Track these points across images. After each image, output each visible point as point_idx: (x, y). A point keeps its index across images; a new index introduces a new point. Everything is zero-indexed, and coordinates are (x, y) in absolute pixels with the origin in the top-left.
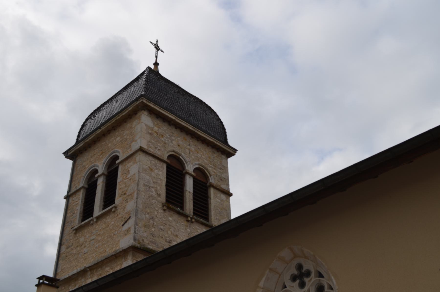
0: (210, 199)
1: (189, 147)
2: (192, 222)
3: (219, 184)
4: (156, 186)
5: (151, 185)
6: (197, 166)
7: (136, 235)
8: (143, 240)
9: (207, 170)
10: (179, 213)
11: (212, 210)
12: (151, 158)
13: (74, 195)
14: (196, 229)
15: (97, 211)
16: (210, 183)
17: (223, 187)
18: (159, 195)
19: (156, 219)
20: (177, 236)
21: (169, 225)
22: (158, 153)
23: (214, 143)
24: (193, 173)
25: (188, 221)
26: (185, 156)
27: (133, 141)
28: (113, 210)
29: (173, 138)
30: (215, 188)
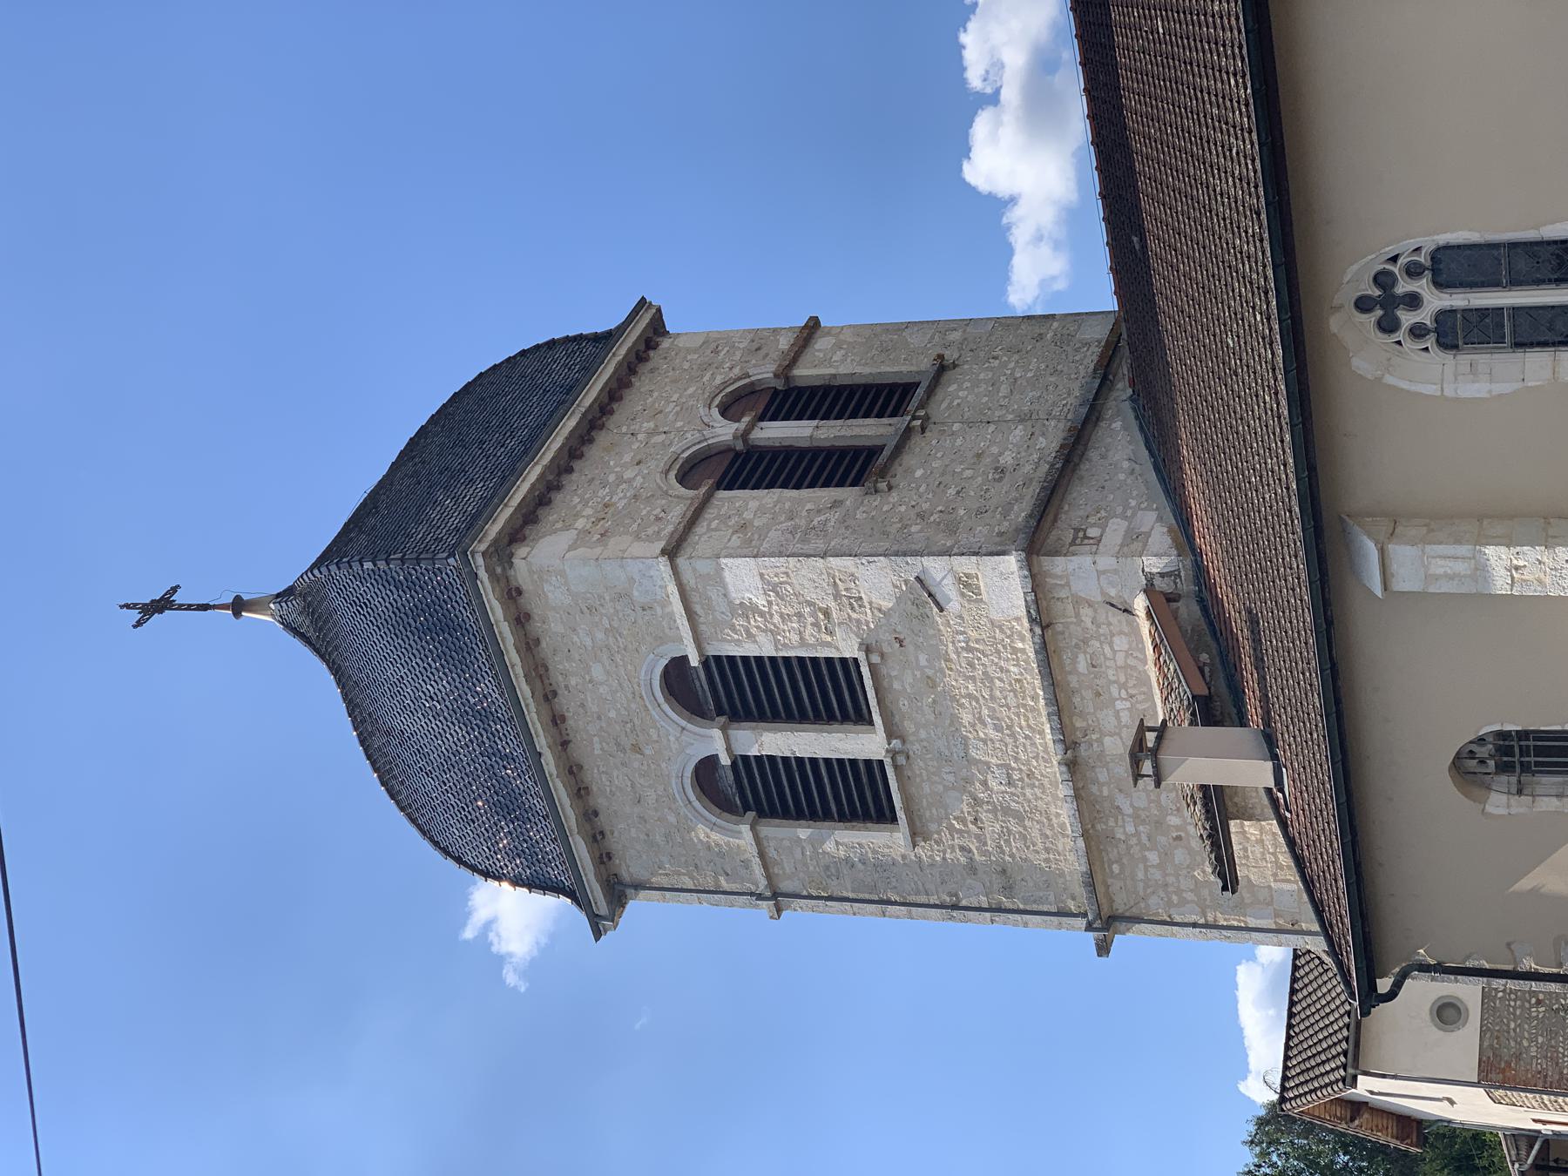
0: (834, 376)
1: (640, 437)
2: (926, 418)
3: (775, 355)
4: (804, 513)
5: (803, 522)
6: (715, 412)
7: (984, 550)
8: (1001, 534)
9: (725, 384)
10: (931, 391)
11: (875, 370)
12: (701, 528)
13: (885, 683)
14: (949, 407)
15: (865, 744)
16: (776, 376)
17: (784, 343)
18: (836, 504)
19: (926, 506)
20: (979, 456)
21: (943, 474)
22: (677, 514)
23: (620, 364)
24: (703, 490)
25: (923, 430)
26: (687, 442)
27: (628, 595)
28: (875, 659)
29: (612, 478)
30: (793, 362)
